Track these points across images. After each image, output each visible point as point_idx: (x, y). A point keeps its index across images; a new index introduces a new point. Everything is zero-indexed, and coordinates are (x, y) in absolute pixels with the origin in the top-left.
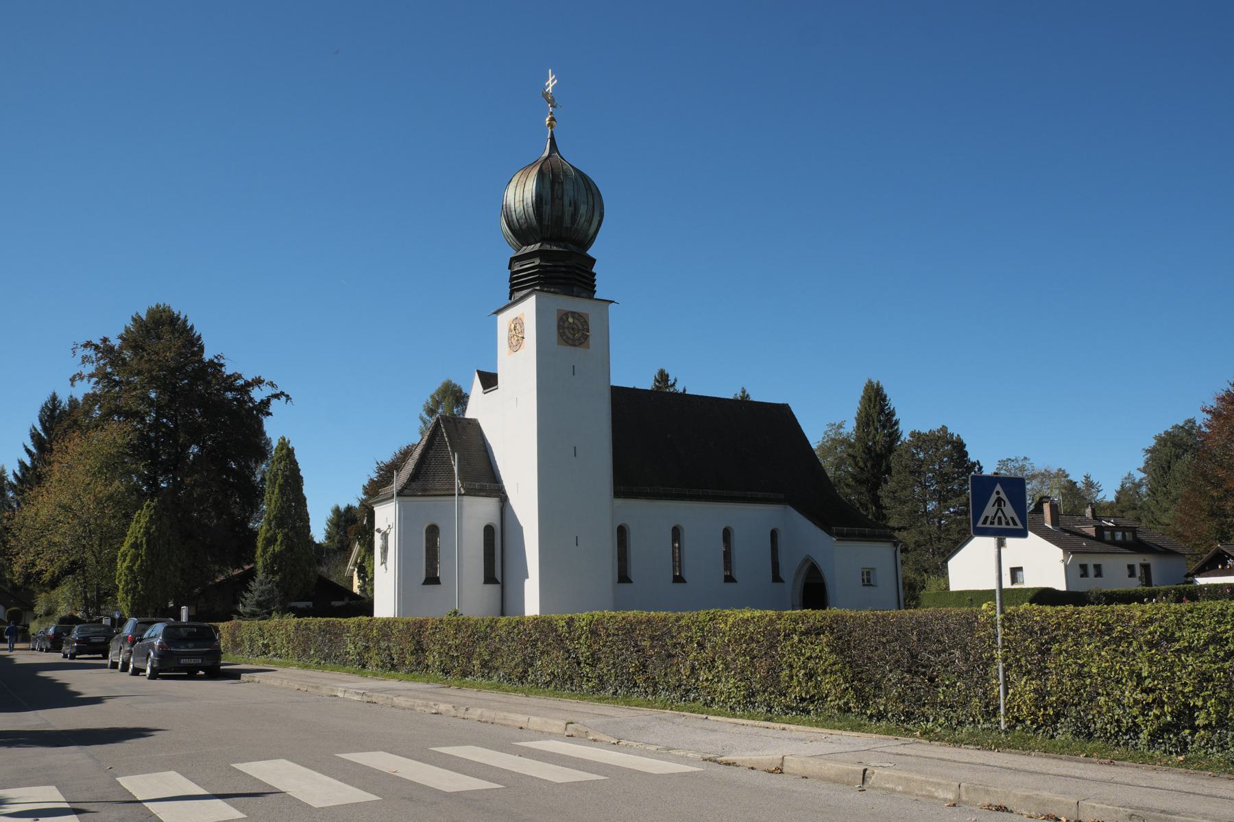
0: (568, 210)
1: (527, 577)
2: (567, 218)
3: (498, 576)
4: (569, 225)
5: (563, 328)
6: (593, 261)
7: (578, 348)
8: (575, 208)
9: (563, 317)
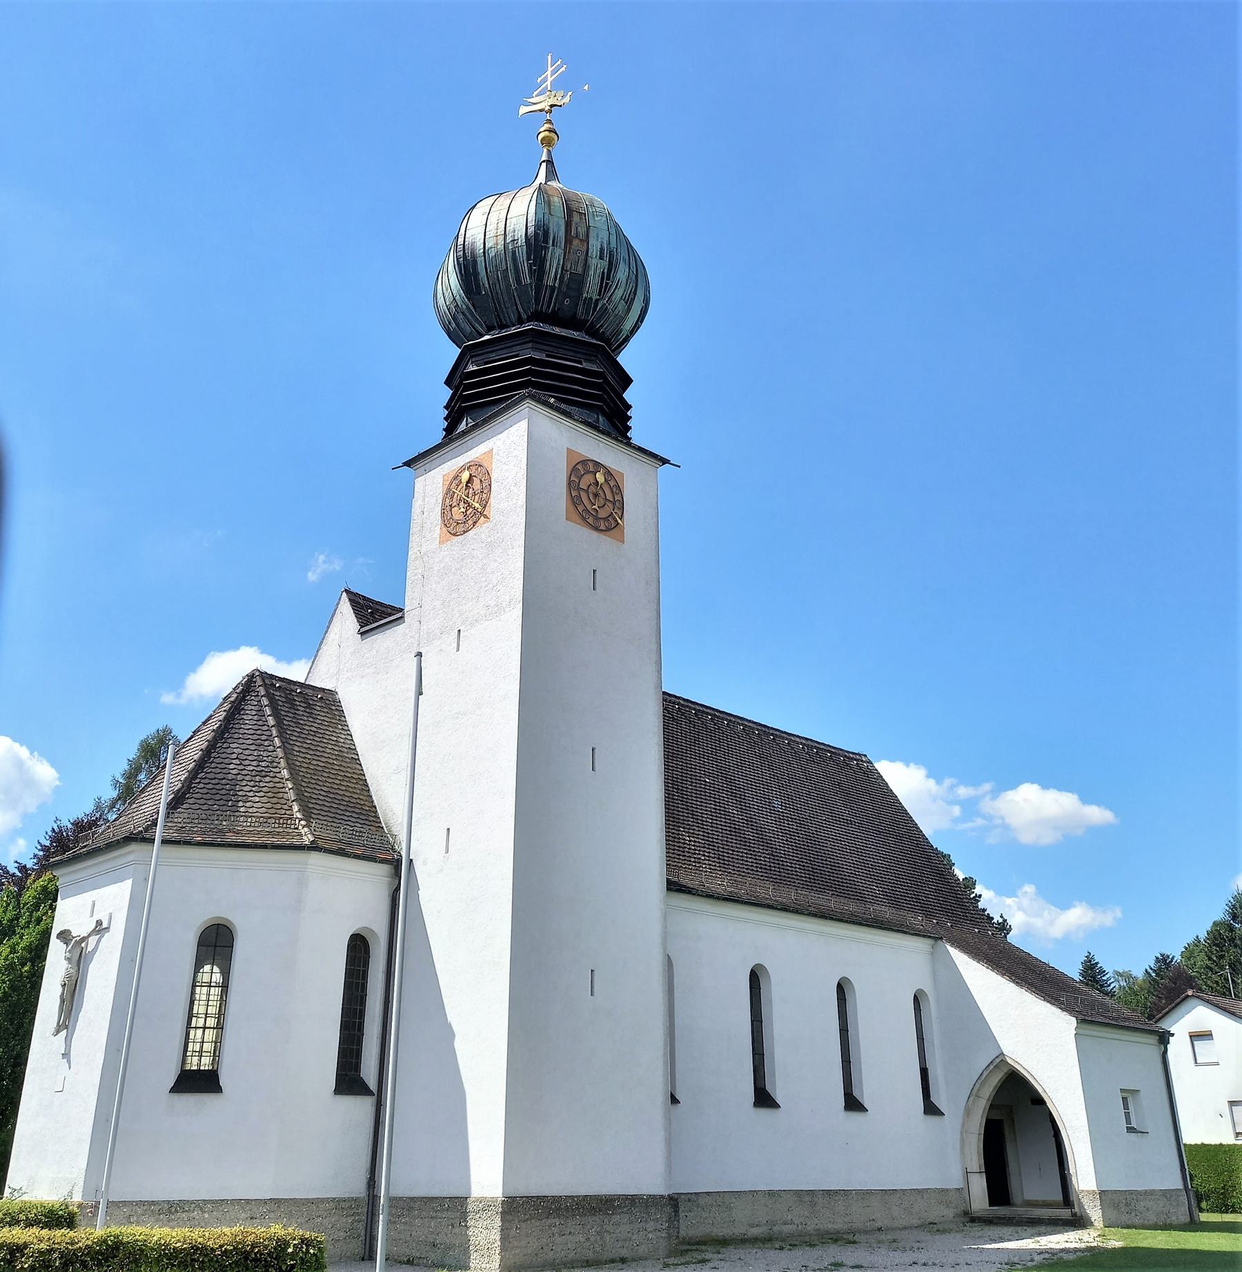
0: (597, 266)
3: (369, 1071)
5: (579, 489)
7: (602, 536)
8: (610, 263)
9: (581, 469)
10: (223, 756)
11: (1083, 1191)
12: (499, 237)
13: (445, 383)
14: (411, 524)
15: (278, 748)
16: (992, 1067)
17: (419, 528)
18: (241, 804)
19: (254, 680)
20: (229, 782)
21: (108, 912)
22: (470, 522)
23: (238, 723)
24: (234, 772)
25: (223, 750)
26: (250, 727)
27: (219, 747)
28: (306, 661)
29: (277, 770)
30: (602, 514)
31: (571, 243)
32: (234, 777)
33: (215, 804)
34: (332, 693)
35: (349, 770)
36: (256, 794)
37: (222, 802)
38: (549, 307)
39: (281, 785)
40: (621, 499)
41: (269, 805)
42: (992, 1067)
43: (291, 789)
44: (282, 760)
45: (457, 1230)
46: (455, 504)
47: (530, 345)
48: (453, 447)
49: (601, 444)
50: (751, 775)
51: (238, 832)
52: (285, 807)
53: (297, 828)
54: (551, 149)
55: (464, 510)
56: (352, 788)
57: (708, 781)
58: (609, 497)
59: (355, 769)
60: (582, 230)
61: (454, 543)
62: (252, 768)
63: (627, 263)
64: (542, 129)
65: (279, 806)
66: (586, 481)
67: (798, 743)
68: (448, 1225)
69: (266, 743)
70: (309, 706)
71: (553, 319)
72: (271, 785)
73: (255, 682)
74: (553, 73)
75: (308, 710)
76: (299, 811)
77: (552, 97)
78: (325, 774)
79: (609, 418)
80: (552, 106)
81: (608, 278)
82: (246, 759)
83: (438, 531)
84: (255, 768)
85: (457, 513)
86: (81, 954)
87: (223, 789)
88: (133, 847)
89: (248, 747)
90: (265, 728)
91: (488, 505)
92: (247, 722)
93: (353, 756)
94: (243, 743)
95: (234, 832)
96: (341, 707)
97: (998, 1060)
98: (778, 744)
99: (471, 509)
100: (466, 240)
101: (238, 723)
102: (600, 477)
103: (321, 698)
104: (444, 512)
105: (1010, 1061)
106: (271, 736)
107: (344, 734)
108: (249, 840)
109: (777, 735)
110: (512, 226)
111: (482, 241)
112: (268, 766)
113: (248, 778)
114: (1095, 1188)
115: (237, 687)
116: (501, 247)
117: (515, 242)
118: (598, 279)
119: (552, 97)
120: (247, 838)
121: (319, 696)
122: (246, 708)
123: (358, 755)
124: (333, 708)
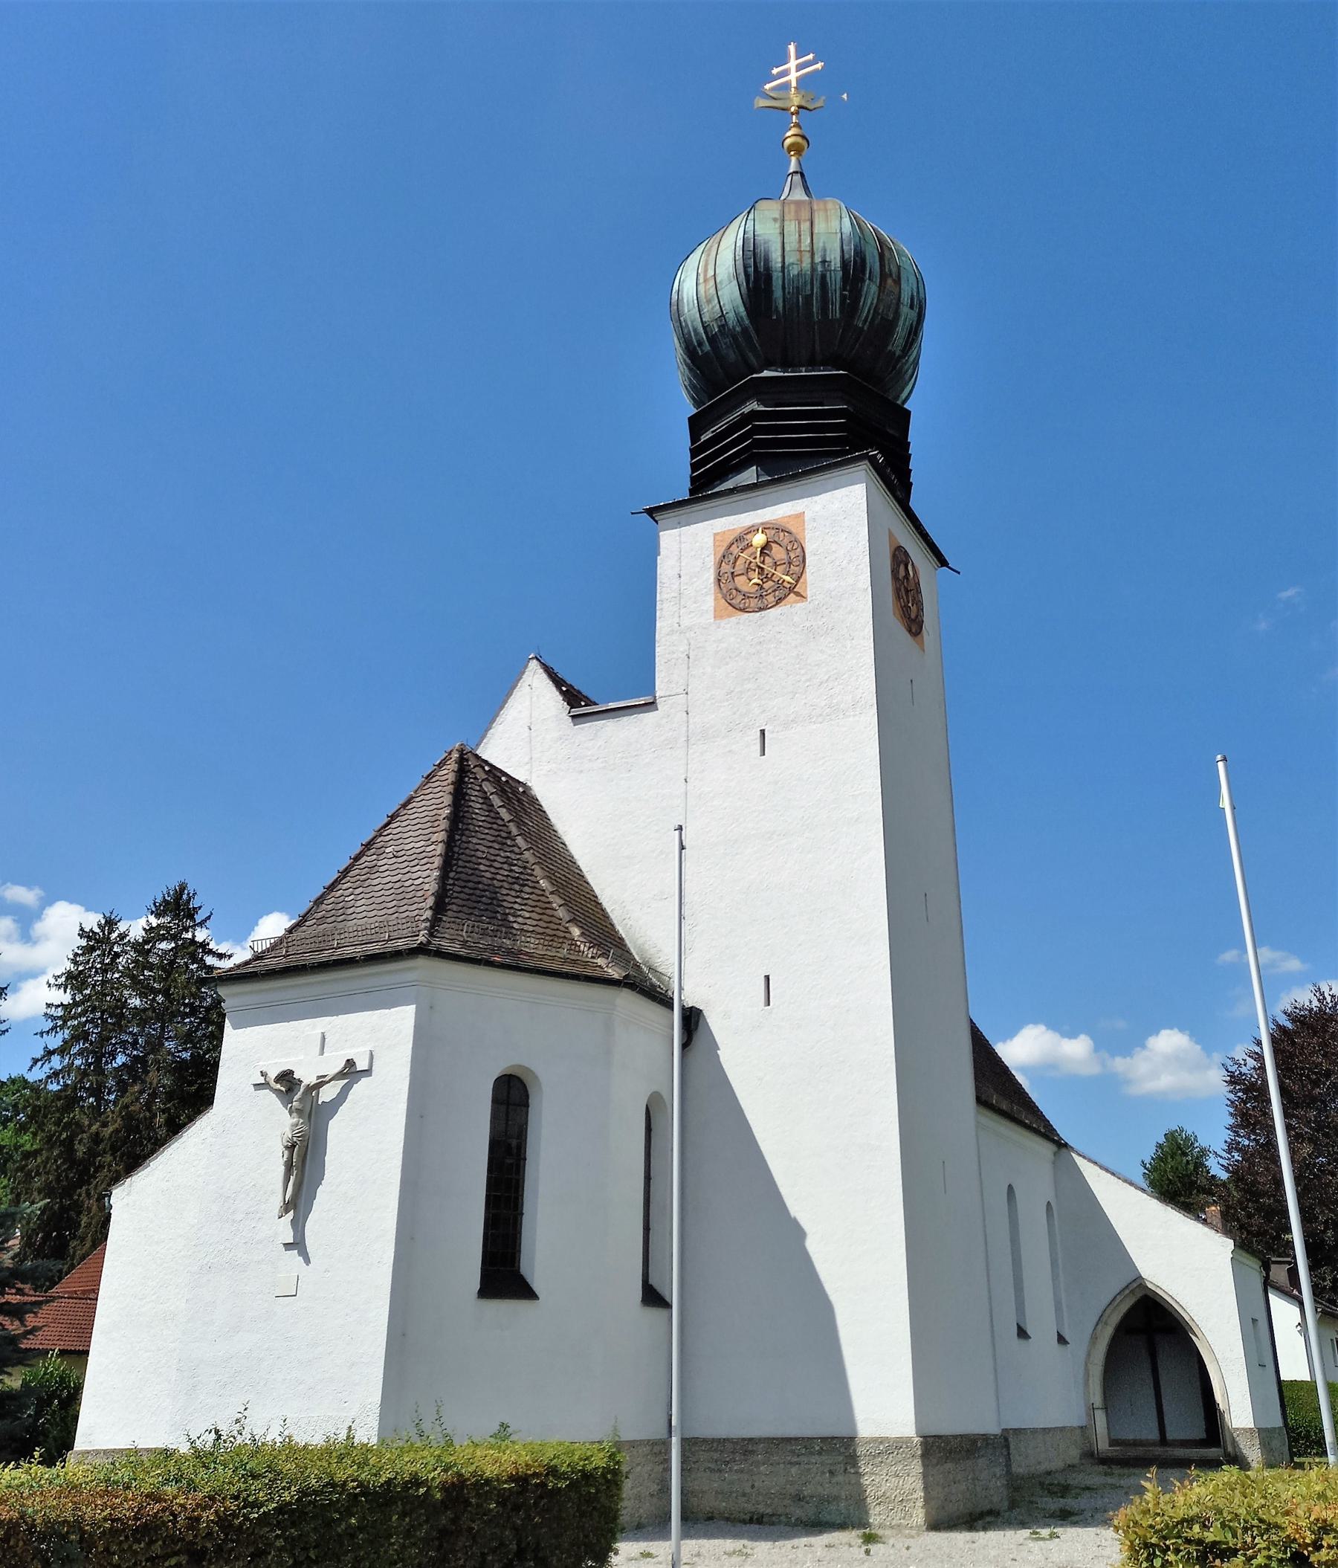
0: (907, 314)
11: (1238, 1429)
16: (1127, 1292)
21: (368, 1049)
22: (771, 599)
42: (1127, 1292)
45: (840, 1478)
48: (731, 500)
60: (894, 270)
61: (741, 621)
68: (823, 1473)
74: (799, 68)
80: (800, 107)
86: (312, 1106)
88: (421, 962)
92: (477, 811)
97: (1135, 1285)
105: (1150, 1286)
110: (821, 245)
114: (1252, 1426)
118: (904, 333)
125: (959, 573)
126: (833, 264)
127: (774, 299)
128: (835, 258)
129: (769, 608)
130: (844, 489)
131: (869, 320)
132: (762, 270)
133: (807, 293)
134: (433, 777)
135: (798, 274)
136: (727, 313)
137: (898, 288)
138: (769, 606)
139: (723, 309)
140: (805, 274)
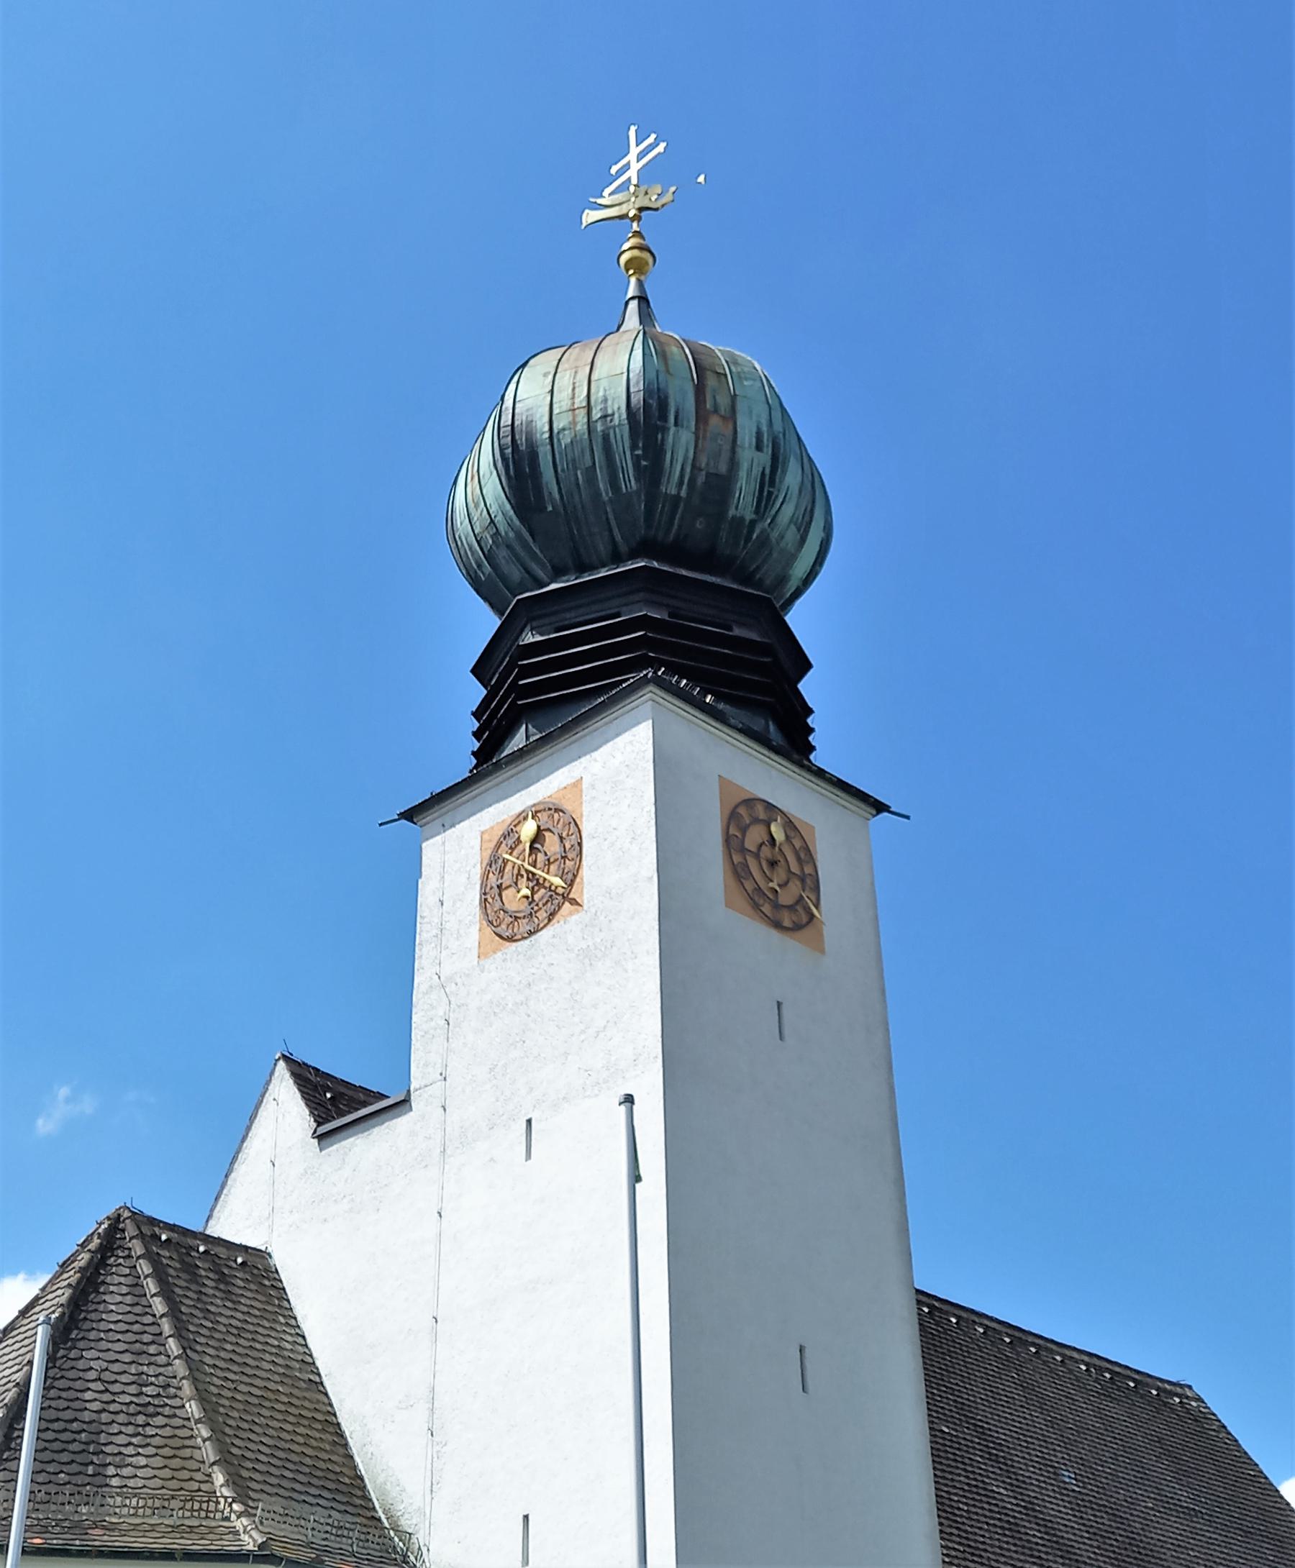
0: (751, 462)
1: (805, 666)
2: (743, 500)
4: (749, 516)
5: (743, 850)
6: (812, 730)
8: (775, 458)
9: (782, 610)
10: (71, 1374)
12: (577, 411)
13: (474, 671)
14: (418, 925)
15: (175, 1358)
17: (434, 932)
18: (111, 1471)
19: (121, 1226)
20: (85, 1426)
22: (542, 915)
23: (96, 1310)
24: (96, 1406)
25: (69, 1364)
26: (120, 1317)
27: (63, 1357)
28: (26, 1277)
29: (176, 1402)
30: (786, 898)
31: (706, 422)
32: (94, 1416)
33: (62, 1472)
34: (262, 1255)
35: (307, 1404)
36: (140, 1450)
37: (74, 1468)
38: (668, 530)
39: (189, 1433)
40: (814, 873)
41: (166, 1473)
43: (208, 1439)
44: (184, 1381)
46: (508, 883)
47: (641, 595)
48: (500, 779)
49: (774, 773)
50: (1013, 1420)
51: (111, 1528)
52: (199, 1476)
53: (228, 1519)
54: (642, 278)
55: (528, 892)
56: (315, 1439)
57: (947, 1430)
58: (795, 868)
59: (318, 1401)
60: (723, 402)
61: (508, 957)
62: (127, 1399)
63: (799, 458)
64: (626, 246)
65: (185, 1474)
66: (754, 836)
67: (1077, 1361)
69: (152, 1349)
70: (222, 1278)
71: (674, 553)
72: (167, 1432)
73: (123, 1231)
74: (640, 156)
75: (222, 1286)
76: (227, 1484)
77: (641, 195)
78: (264, 1412)
79: (781, 727)
80: (641, 209)
81: (772, 483)
82: (116, 1381)
83: (474, 931)
84: (134, 1399)
85: (514, 899)
87: (75, 1440)
89: (118, 1357)
90: (149, 1319)
91: (578, 880)
92: (113, 1307)
93: (312, 1377)
94: (109, 1350)
95: (104, 1528)
96: (281, 1281)
98: (1045, 1363)
99: (543, 891)
100: (516, 417)
101: (96, 1310)
102: (777, 831)
103: (243, 1263)
104: (486, 900)
106: (161, 1334)
107: (291, 1335)
108: (138, 1543)
109: (1046, 1345)
110: (601, 394)
111: (546, 419)
112: (159, 1395)
113: (121, 1418)
115: (88, 1240)
116: (581, 426)
117: (609, 419)
119: (641, 195)
120: (133, 1539)
121: (240, 1260)
122: (109, 1279)
123: (319, 1375)
124: (267, 1283)
125: (908, 817)
126: (616, 416)
127: (544, 482)
128: (618, 404)
129: (542, 928)
130: (627, 733)
131: (686, 481)
132: (524, 448)
133: (587, 466)
134: (73, 1262)
135: (572, 442)
136: (495, 517)
137: (731, 426)
138: (541, 925)
139: (491, 512)
140: (581, 440)
